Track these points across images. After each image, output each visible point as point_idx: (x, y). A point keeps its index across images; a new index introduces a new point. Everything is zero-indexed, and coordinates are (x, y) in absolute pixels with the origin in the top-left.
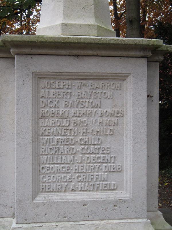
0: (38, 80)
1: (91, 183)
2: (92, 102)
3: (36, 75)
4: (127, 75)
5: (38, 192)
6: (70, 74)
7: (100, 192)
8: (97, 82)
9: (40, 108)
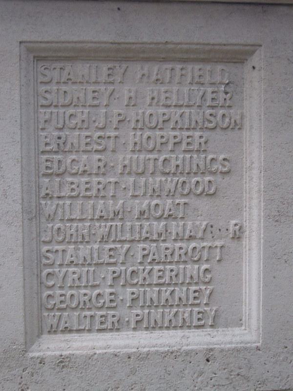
0: (35, 61)
1: (84, 313)
2: (151, 115)
3: (29, 50)
4: (252, 48)
5: (40, 333)
6: (59, 45)
7: (194, 330)
8: (88, 65)
9: (39, 130)
